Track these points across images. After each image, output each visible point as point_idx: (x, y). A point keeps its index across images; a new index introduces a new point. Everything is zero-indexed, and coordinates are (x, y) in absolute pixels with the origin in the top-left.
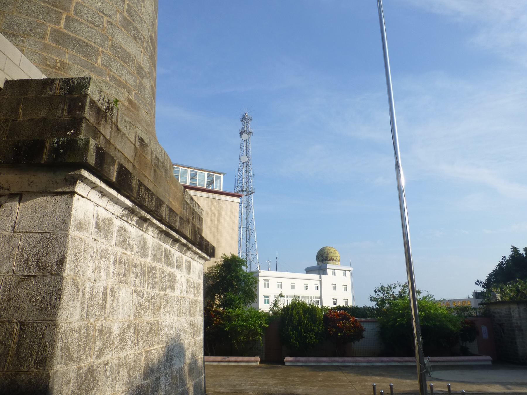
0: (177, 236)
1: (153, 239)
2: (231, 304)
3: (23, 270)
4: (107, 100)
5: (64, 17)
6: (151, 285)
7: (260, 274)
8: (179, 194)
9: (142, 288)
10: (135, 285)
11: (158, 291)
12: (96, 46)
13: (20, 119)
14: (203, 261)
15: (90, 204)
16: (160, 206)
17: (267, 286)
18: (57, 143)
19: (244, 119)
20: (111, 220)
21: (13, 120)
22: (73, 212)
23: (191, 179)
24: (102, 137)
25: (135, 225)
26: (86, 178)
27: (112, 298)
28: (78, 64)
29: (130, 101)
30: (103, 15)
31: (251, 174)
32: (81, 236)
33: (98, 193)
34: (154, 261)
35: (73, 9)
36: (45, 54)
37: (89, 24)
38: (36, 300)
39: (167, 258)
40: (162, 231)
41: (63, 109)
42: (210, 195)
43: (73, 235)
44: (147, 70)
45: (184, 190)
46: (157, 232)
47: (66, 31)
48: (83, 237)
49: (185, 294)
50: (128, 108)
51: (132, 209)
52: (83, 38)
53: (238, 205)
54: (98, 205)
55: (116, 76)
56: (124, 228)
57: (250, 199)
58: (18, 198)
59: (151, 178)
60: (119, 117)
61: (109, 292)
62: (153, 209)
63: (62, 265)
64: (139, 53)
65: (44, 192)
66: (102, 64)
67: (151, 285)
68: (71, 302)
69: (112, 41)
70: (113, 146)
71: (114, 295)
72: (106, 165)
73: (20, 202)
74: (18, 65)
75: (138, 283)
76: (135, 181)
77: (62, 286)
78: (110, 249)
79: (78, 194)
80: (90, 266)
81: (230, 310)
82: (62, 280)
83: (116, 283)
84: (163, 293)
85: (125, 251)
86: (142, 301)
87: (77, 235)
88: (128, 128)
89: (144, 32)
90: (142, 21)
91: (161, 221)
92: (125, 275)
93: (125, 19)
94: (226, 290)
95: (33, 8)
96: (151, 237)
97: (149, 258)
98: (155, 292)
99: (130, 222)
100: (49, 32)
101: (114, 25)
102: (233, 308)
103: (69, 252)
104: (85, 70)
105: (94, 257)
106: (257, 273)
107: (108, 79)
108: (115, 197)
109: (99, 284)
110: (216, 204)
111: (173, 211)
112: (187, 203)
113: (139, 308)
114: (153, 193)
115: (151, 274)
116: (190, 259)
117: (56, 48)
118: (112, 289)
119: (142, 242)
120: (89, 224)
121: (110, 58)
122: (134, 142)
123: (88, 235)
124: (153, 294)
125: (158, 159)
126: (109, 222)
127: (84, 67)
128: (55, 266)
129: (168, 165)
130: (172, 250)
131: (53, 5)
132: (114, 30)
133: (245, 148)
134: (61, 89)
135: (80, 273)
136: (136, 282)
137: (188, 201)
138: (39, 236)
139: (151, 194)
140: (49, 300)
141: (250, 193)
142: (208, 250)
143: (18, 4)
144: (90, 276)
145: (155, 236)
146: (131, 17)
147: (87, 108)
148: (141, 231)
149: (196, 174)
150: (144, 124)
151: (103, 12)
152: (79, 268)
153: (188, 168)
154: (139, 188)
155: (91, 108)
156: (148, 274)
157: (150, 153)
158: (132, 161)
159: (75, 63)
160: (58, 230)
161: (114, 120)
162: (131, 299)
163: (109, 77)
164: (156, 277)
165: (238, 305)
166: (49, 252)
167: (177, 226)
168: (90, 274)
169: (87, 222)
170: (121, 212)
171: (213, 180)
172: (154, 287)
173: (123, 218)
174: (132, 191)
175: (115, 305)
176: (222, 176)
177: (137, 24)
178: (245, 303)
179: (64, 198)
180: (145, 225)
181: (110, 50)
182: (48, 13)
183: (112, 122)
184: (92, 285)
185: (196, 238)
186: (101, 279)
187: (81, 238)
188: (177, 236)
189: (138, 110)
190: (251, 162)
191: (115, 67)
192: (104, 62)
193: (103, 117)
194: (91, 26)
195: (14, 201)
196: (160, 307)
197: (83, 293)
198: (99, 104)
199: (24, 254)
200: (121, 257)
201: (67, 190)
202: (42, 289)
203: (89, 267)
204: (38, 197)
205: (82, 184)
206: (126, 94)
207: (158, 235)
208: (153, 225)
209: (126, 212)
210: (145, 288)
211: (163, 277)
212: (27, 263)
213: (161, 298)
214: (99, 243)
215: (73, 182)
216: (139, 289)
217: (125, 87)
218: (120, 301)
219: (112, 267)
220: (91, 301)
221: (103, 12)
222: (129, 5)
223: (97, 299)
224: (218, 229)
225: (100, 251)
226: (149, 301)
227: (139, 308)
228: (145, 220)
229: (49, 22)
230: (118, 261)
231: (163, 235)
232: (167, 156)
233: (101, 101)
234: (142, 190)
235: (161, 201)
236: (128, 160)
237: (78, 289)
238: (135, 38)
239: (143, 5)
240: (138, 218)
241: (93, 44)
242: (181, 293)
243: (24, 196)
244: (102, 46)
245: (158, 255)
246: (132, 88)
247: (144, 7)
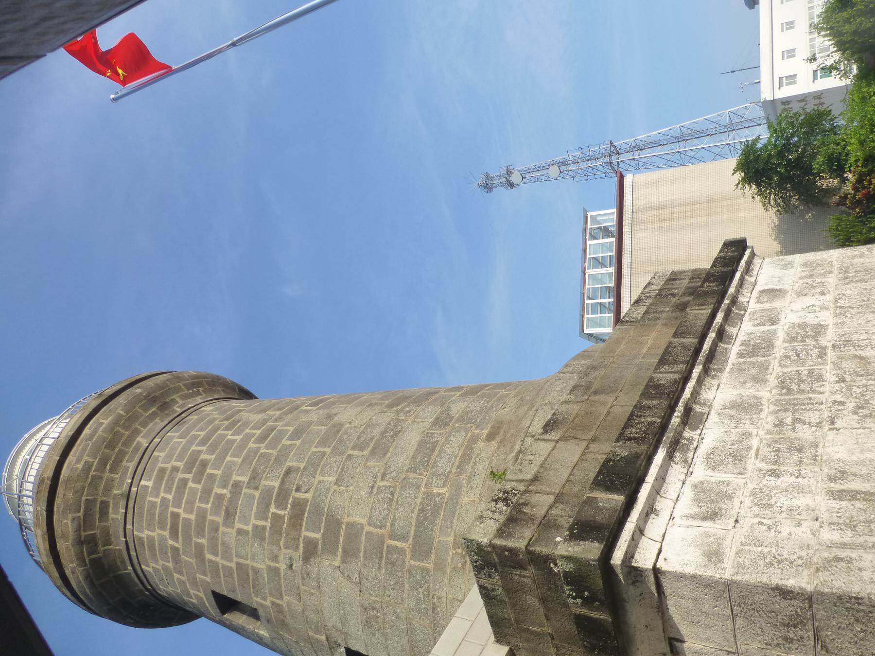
0: (712, 335)
1: (722, 386)
2: (838, 160)
3: (805, 646)
4: (493, 504)
5: (393, 543)
6: (816, 386)
7: (769, 98)
8: (631, 332)
9: (823, 407)
10: (819, 425)
11: (828, 367)
12: (420, 496)
13: (548, 630)
14: (757, 261)
15: (670, 537)
16: (657, 387)
17: (792, 79)
18: (575, 598)
19: (488, 187)
20: (695, 487)
21: (553, 638)
22: (689, 570)
23: (603, 265)
24: (554, 511)
25: (699, 431)
26: (626, 552)
27: (850, 478)
28: (452, 522)
29: (490, 437)
30: (376, 488)
31: (578, 153)
32: (733, 553)
33: (650, 521)
34: (765, 381)
35: (378, 530)
36: (449, 570)
37: (393, 507)
38: (862, 631)
39: (757, 349)
40: (706, 371)
41: (520, 575)
42: (626, 229)
43: (732, 571)
44: (438, 410)
45: (622, 322)
46: (708, 381)
47: (411, 540)
48: (734, 549)
49: (829, 297)
50: (502, 441)
51: (671, 446)
52: (415, 516)
53: (637, 176)
54: (671, 518)
55: (457, 463)
56: (709, 456)
57: (624, 146)
58: (678, 644)
59: (610, 399)
60: (515, 477)
61: (837, 486)
62: (665, 403)
63: (792, 592)
64: (415, 426)
65: (661, 609)
66: (444, 486)
67: (816, 386)
68: (864, 573)
69: (407, 471)
70: (564, 486)
71: (843, 475)
72: (598, 518)
73: (683, 641)
74: (471, 623)
75: (812, 417)
76: (618, 451)
77: (832, 593)
78: (751, 486)
79: (657, 560)
80: (788, 531)
81: (853, 159)
82: (822, 594)
83: (817, 469)
84: (831, 355)
85: (753, 452)
86: (851, 405)
87: (731, 562)
88: (532, 457)
89: (386, 418)
90: (369, 425)
91: (686, 379)
92: (800, 450)
93: (373, 452)
94: (808, 171)
95: (392, 583)
96: (720, 392)
97: (761, 394)
98: (829, 373)
99: (695, 444)
100: (417, 563)
101: (386, 469)
102: (847, 155)
103: (765, 579)
104: (457, 513)
105: (769, 522)
106: (766, 105)
107: (464, 476)
108: (653, 486)
109: (823, 509)
110: (641, 216)
111: (664, 355)
112: (646, 312)
113: (865, 412)
114: (635, 406)
115: (794, 387)
116: (755, 294)
117: (436, 553)
118: (832, 479)
119: (732, 412)
120: (708, 536)
121: (433, 474)
122: (553, 444)
123: (730, 537)
124: (835, 378)
125: (575, 387)
126: (700, 489)
127: (454, 513)
128: (795, 602)
129: (583, 362)
130: (741, 338)
131: (381, 557)
132: (392, 469)
133: (535, 174)
134: (490, 576)
135: (803, 553)
136: (813, 421)
137: (642, 310)
138: (739, 622)
139: (638, 410)
140: (862, 614)
141: (613, 148)
142: (735, 252)
143: (393, 601)
144: (809, 532)
145: (715, 382)
146: (368, 444)
147: (511, 543)
148: (710, 417)
149: (594, 258)
150: (522, 411)
151: (372, 487)
152: (795, 557)
153: (585, 274)
154: (630, 439)
155: (510, 535)
156: (794, 394)
157: (567, 406)
158: (585, 444)
159: (451, 527)
160: (726, 595)
161: (522, 487)
162: (847, 432)
163: (461, 473)
164: (799, 373)
165: (838, 144)
166: (769, 609)
167: (692, 341)
168: (804, 532)
169: (705, 539)
170: (679, 466)
171: (599, 228)
172: (820, 378)
173: (690, 459)
174: (637, 456)
175: (864, 471)
176: (590, 214)
177: (377, 432)
178: (833, 130)
179: (666, 583)
180: (698, 408)
181: (421, 474)
182: (393, 564)
183: (526, 492)
184: (826, 526)
185: (713, 292)
186: (812, 504)
187: (737, 553)
188: (712, 335)
189: (502, 422)
190: (558, 159)
191: (444, 465)
192: (441, 483)
193: (520, 511)
194: (394, 504)
195: (683, 649)
196: (861, 358)
197: (844, 546)
198: (502, 518)
199: (775, 642)
200: (765, 460)
201: (652, 579)
202: (841, 623)
203: (790, 534)
204: (670, 618)
205: (637, 556)
206: (481, 444)
207: (713, 377)
208: (695, 393)
209: (678, 456)
210: (822, 398)
211: (798, 355)
212: (792, 639)
213: (842, 358)
214: (742, 511)
215: (635, 573)
216: (826, 415)
217: (469, 448)
218: (854, 458)
219: (787, 480)
220: (860, 528)
221: (372, 487)
222: (353, 448)
223: (854, 514)
224: (687, 204)
225: (756, 510)
226: (850, 388)
227: (865, 412)
228: (688, 410)
229: (404, 562)
230: (773, 467)
231: (712, 366)
232: (566, 366)
233: (496, 516)
234: (632, 432)
235: (648, 386)
236: (584, 453)
237: (838, 559)
238: (396, 434)
239: (348, 425)
240: (687, 429)
241: (419, 501)
242: (827, 309)
243: (671, 635)
244: (418, 487)
245: (754, 371)
246: (470, 434)
247: (350, 423)
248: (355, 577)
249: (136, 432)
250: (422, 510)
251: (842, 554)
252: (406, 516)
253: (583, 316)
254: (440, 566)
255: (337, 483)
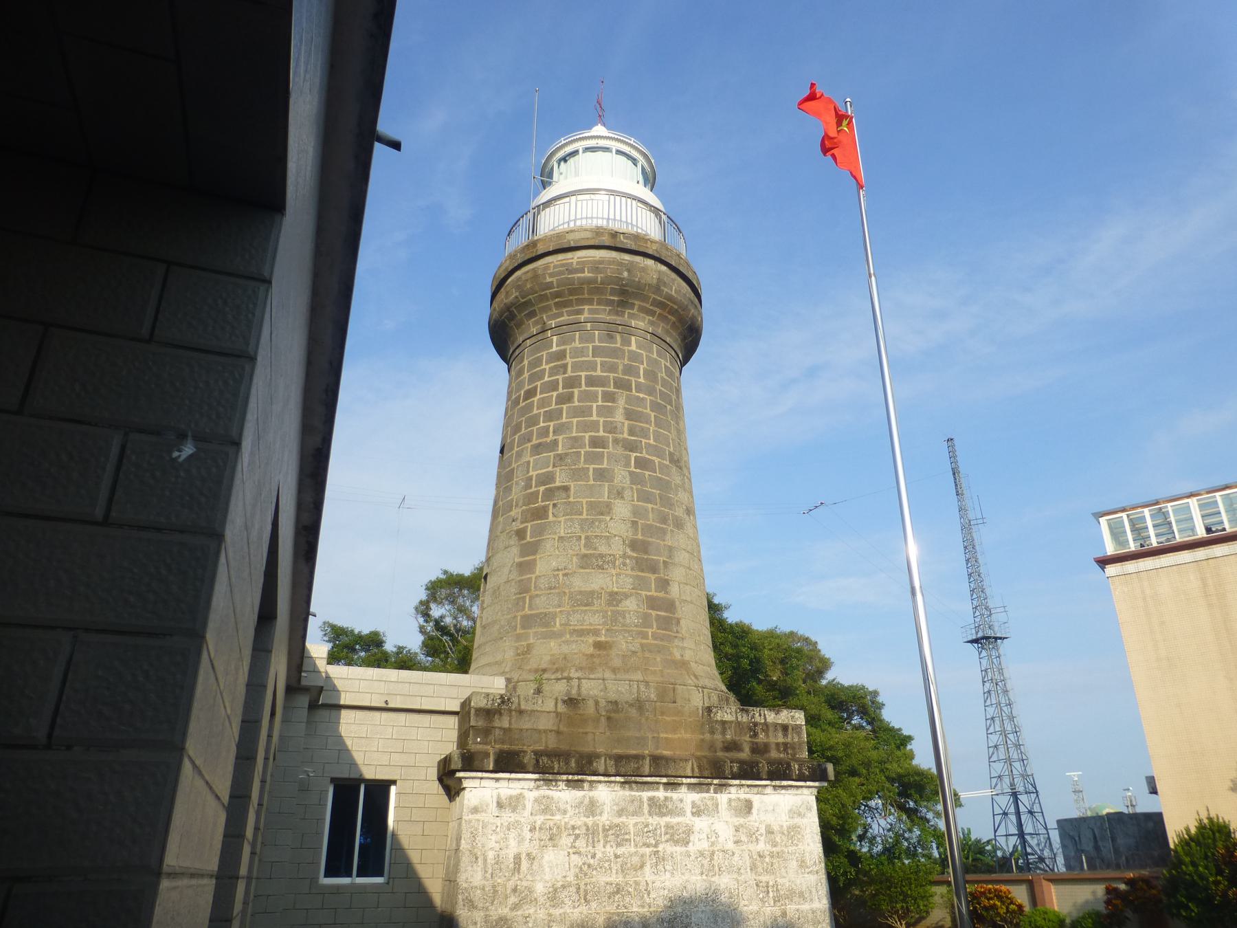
75: (581, 843)
177: (603, 549)
197: (485, 860)
208: (600, 782)
219: (528, 835)
248: (512, 577)
249: (590, 302)
250: (546, 614)
251: (480, 861)
252: (543, 604)
253: (1123, 510)
254: (519, 638)
255: (561, 538)
